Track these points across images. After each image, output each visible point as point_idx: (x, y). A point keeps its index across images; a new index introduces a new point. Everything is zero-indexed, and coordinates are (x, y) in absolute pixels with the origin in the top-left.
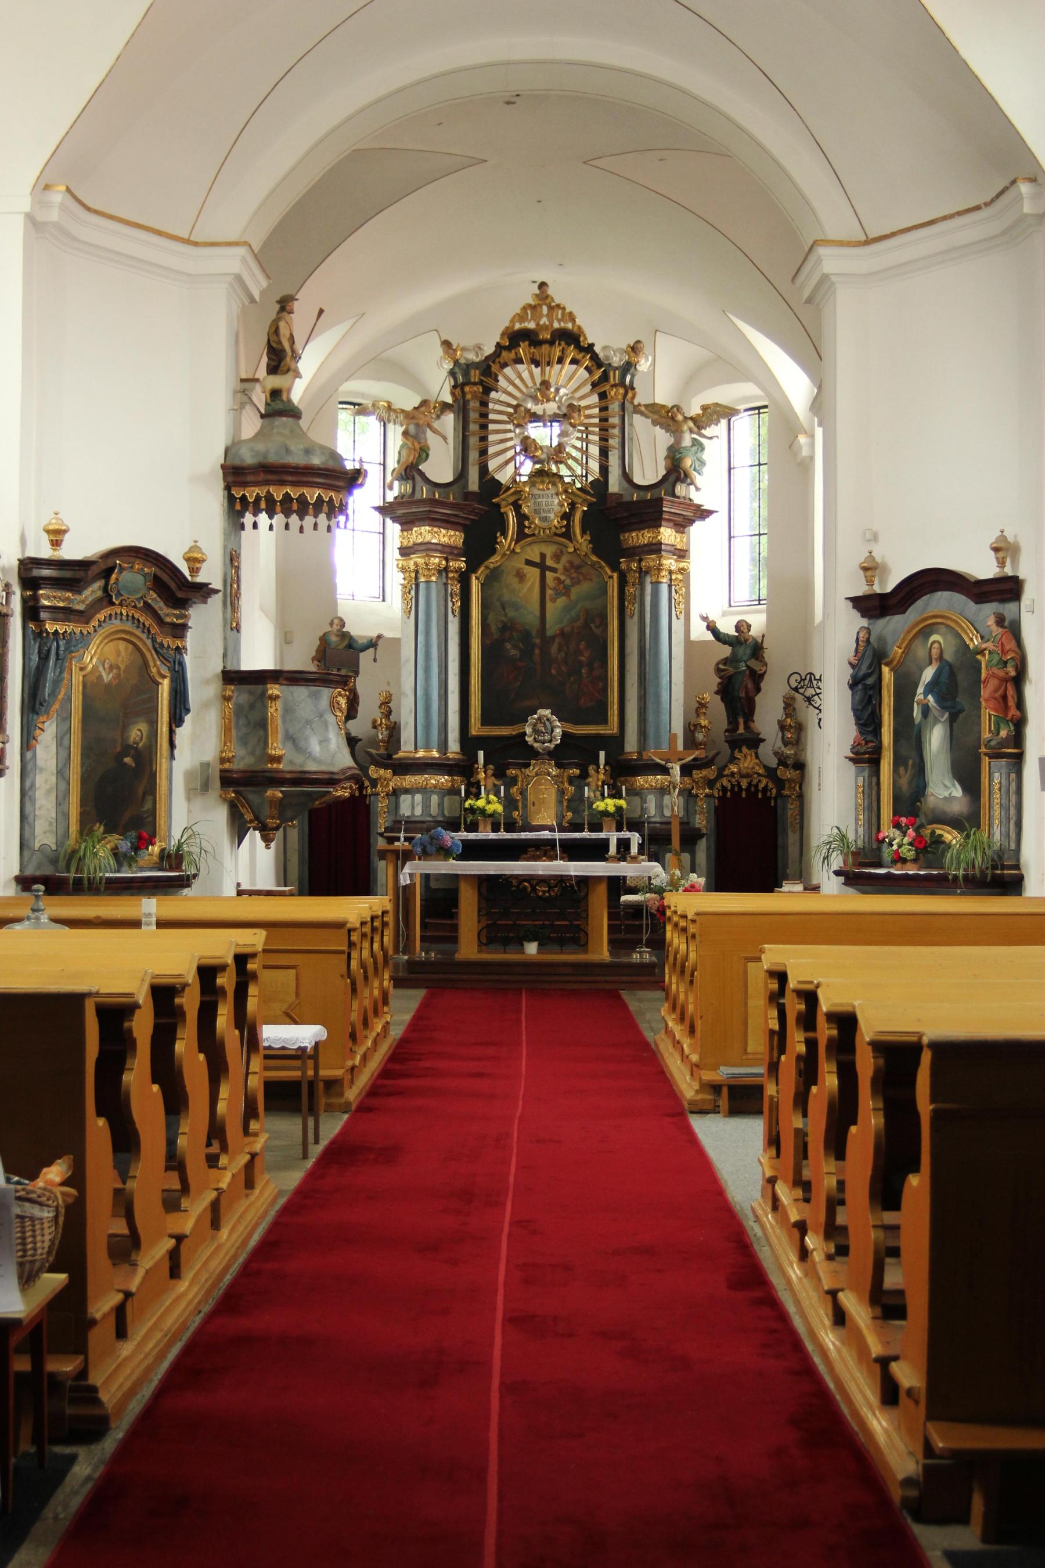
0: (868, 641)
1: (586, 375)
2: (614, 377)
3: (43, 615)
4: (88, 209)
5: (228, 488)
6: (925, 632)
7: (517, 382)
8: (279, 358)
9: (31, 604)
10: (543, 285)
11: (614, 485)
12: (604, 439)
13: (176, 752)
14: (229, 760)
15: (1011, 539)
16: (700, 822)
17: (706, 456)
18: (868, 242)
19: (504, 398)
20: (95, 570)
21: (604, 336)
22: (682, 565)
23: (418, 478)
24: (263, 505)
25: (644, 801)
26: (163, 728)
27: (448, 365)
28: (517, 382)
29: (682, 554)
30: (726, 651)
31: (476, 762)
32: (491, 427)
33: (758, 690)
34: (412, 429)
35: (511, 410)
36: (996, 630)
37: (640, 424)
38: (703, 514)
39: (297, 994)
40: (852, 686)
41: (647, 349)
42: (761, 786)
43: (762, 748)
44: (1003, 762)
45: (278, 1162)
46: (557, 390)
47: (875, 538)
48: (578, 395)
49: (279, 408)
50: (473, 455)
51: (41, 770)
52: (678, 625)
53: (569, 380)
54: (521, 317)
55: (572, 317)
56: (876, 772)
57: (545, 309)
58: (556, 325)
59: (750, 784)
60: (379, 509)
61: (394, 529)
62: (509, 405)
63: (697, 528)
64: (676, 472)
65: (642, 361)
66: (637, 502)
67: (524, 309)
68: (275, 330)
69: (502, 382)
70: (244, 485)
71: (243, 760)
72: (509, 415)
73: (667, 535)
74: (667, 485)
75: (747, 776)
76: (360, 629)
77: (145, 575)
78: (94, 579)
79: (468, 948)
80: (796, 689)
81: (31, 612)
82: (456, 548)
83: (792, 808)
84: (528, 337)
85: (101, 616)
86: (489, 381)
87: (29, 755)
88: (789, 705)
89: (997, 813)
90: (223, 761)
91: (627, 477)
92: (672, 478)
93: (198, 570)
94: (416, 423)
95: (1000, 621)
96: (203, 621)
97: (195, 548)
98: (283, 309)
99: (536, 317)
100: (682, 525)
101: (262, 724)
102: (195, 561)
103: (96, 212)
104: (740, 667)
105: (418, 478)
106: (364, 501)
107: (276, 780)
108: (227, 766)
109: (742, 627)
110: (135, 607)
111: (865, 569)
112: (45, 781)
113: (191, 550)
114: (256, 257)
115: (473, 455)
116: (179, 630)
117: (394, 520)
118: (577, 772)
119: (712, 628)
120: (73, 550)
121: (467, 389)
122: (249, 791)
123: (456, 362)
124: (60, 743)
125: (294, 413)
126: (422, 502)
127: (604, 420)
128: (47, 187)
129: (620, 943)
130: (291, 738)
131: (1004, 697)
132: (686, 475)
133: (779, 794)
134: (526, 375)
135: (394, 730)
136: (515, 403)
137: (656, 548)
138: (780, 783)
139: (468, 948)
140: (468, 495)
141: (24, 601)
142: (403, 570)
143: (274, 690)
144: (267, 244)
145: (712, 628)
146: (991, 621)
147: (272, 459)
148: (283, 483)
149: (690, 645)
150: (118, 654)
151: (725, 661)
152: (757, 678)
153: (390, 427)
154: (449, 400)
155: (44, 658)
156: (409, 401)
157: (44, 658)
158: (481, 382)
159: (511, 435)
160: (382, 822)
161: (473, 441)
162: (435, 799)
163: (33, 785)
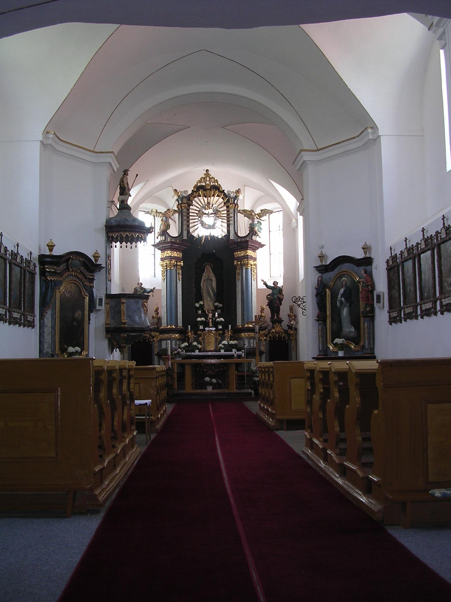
0: (321, 281)
1: (222, 200)
2: (231, 201)
3: (47, 274)
4: (61, 140)
5: (107, 233)
6: (341, 277)
7: (199, 203)
8: (124, 191)
9: (42, 270)
10: (207, 171)
11: (232, 237)
12: (228, 221)
13: (90, 321)
14: (108, 324)
15: (368, 245)
16: (263, 348)
17: (262, 227)
18: (318, 150)
19: (195, 208)
20: (64, 259)
21: (227, 187)
22: (255, 263)
23: (167, 235)
24: (119, 239)
25: (244, 342)
26: (86, 313)
27: (176, 197)
28: (199, 203)
29: (255, 259)
30: (270, 291)
31: (188, 329)
32: (191, 218)
33: (281, 304)
34: (164, 218)
35: (197, 212)
36: (365, 275)
37: (240, 216)
38: (262, 246)
39: (139, 393)
40: (316, 296)
41: (242, 191)
42: (283, 336)
43: (283, 323)
44: (368, 319)
45: (132, 451)
46: (212, 205)
47: (323, 247)
48: (219, 207)
49: (124, 207)
50: (185, 227)
51: (46, 326)
52: (254, 283)
53: (217, 201)
54: (200, 181)
55: (217, 181)
56: (325, 325)
57: (208, 179)
58: (212, 184)
59: (279, 335)
60: (153, 245)
61: (158, 252)
62: (197, 210)
63: (259, 251)
64: (252, 232)
65: (241, 195)
66: (240, 242)
67: (201, 179)
68: (122, 181)
69: (194, 203)
70: (113, 232)
71: (114, 325)
72: (197, 213)
73: (250, 252)
74: (250, 236)
75: (278, 333)
76: (147, 286)
77: (80, 261)
78: (63, 263)
79: (189, 389)
80: (295, 302)
81: (43, 273)
82: (179, 258)
83: (293, 344)
84: (202, 187)
85: (66, 275)
86: (190, 202)
87: (42, 321)
88: (291, 309)
89: (366, 336)
90: (106, 324)
91: (236, 234)
92: (251, 234)
93: (98, 260)
94: (166, 216)
95: (366, 272)
96: (99, 277)
97: (97, 253)
98: (125, 174)
99: (205, 182)
100: (254, 249)
101: (119, 312)
102: (96, 257)
103: (63, 141)
104: (275, 296)
105: (167, 235)
106: (151, 239)
107: (124, 330)
108: (108, 326)
109: (275, 283)
110: (77, 272)
111: (319, 257)
112: (47, 330)
113: (95, 253)
114: (116, 157)
115: (185, 227)
116: (92, 280)
117: (158, 249)
118: (221, 332)
119: (265, 284)
120: (57, 252)
121: (183, 205)
122: (115, 335)
123: (179, 196)
124: (52, 318)
125: (129, 208)
126: (168, 242)
127: (228, 215)
128: (48, 132)
129: (240, 385)
130: (129, 317)
131: (368, 297)
132: (256, 233)
133: (289, 339)
134: (202, 201)
135: (159, 319)
136: (198, 209)
137: (247, 257)
138: (289, 335)
139: (189, 389)
140: (183, 240)
141: (40, 269)
142: (162, 265)
143: (124, 300)
144: (120, 152)
145: (265, 284)
146: (363, 272)
147: (122, 223)
148: (126, 231)
149: (258, 290)
150: (71, 288)
151: (269, 295)
152: (281, 300)
153: (156, 218)
154: (176, 209)
155: (47, 289)
156: (163, 210)
157: (47, 289)
158: (187, 203)
159: (197, 220)
160: (156, 351)
161: (185, 222)
162: (174, 342)
163: (44, 331)
